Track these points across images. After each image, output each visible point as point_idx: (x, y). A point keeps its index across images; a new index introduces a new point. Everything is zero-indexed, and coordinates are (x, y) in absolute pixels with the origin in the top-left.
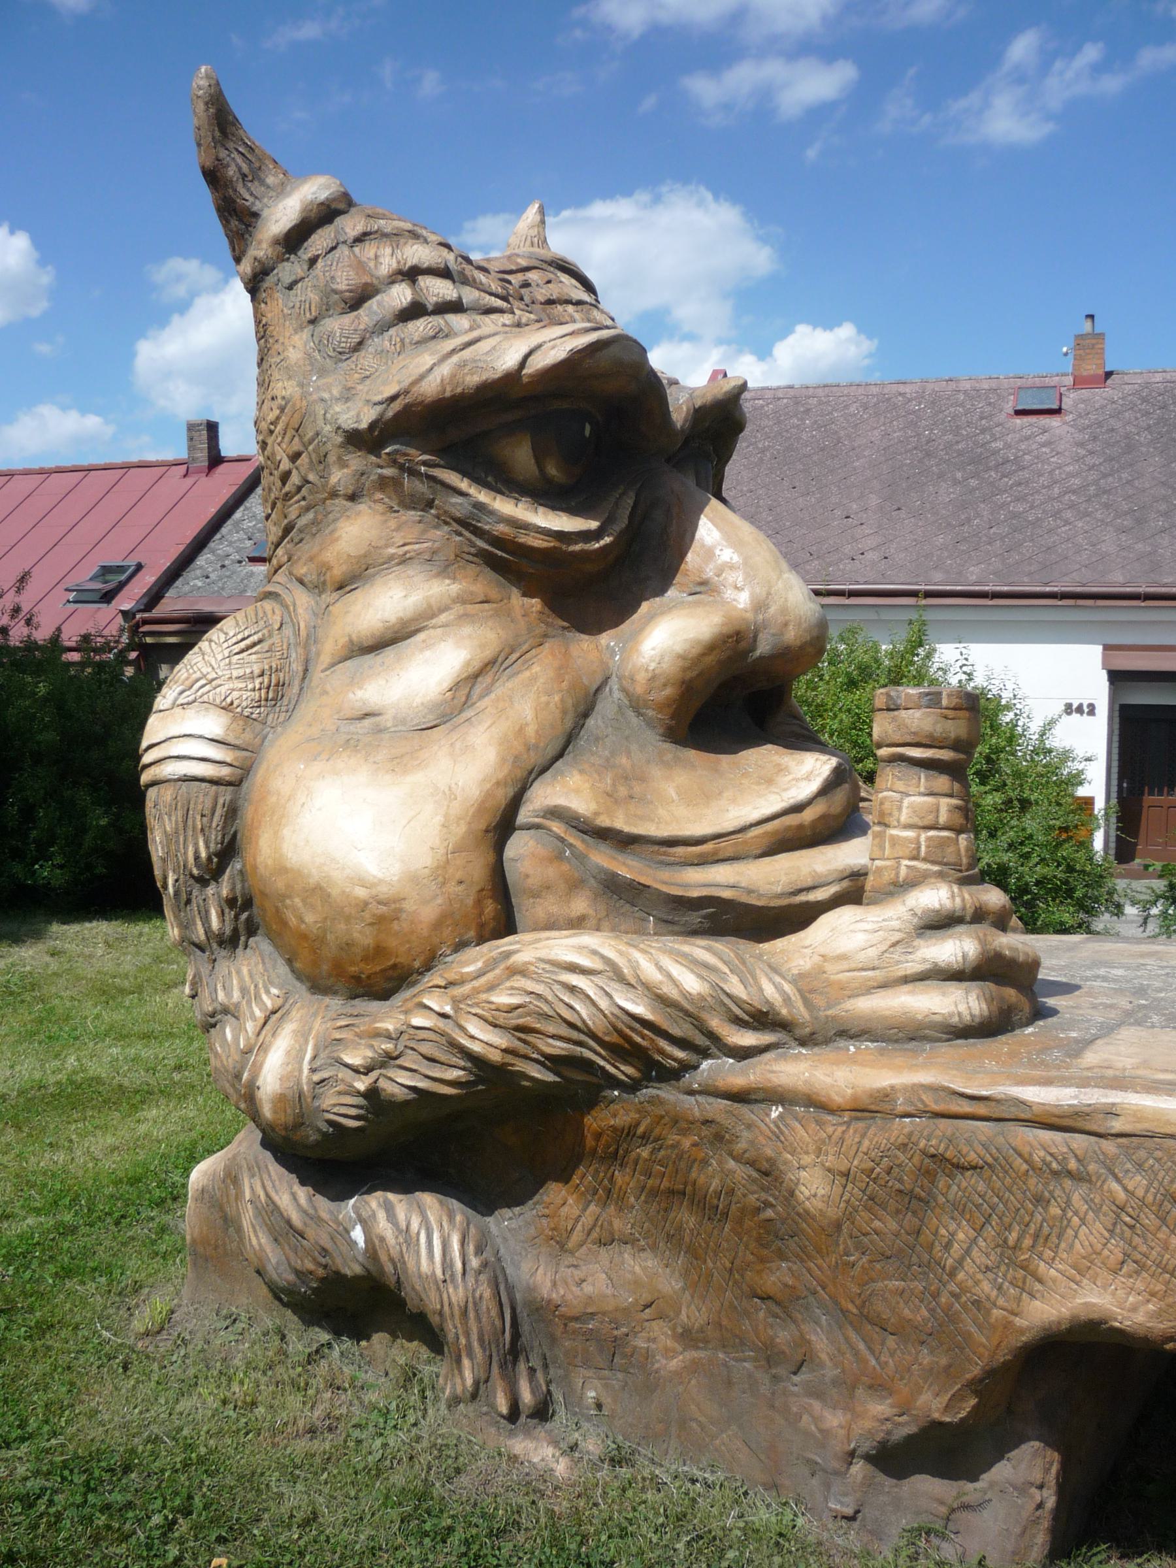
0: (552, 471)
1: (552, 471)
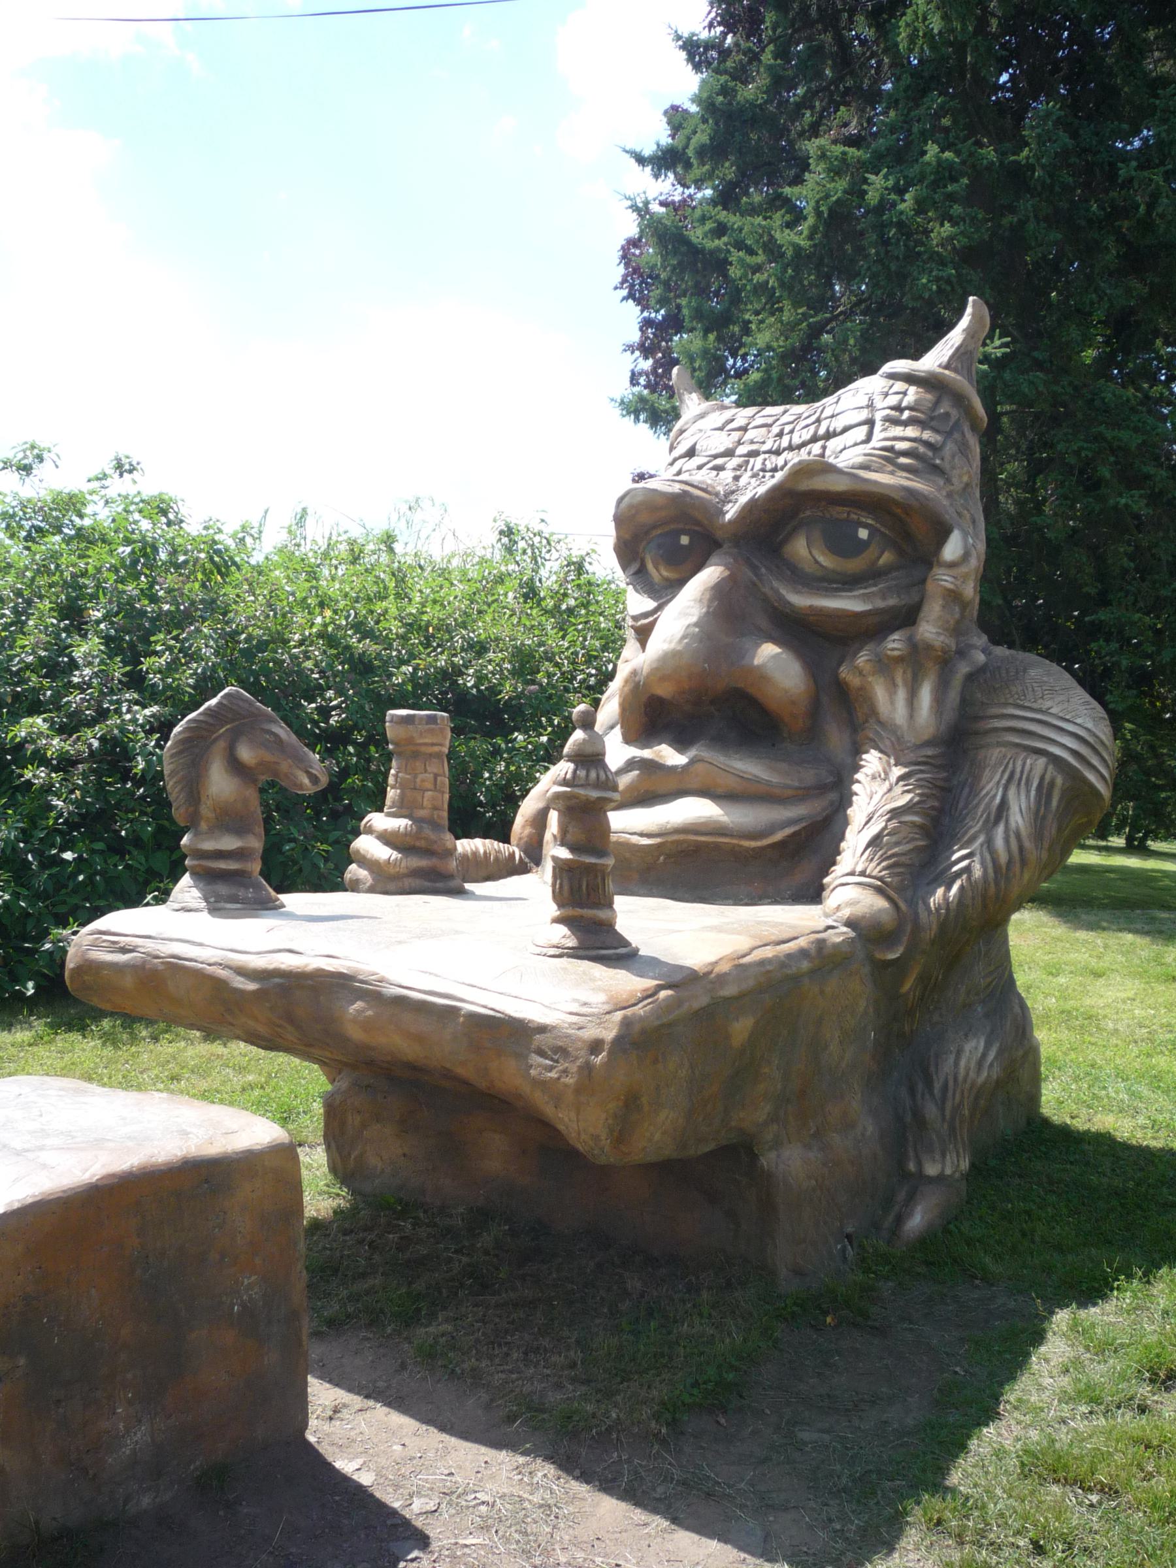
0: (665, 574)
1: (665, 574)
